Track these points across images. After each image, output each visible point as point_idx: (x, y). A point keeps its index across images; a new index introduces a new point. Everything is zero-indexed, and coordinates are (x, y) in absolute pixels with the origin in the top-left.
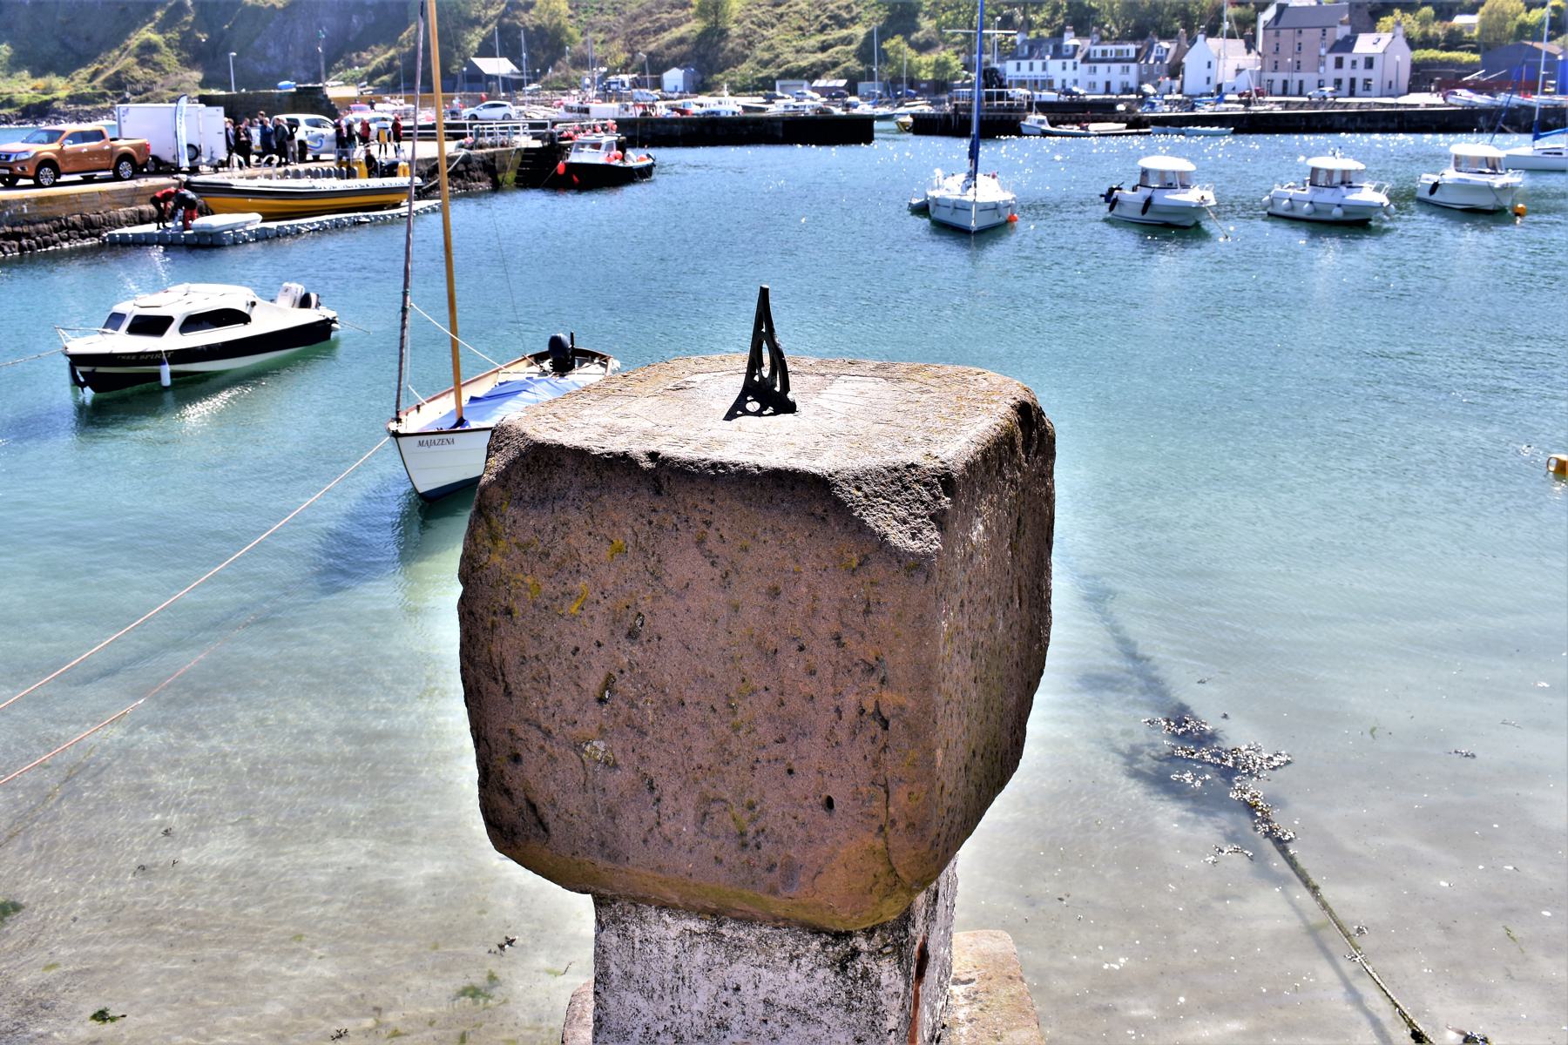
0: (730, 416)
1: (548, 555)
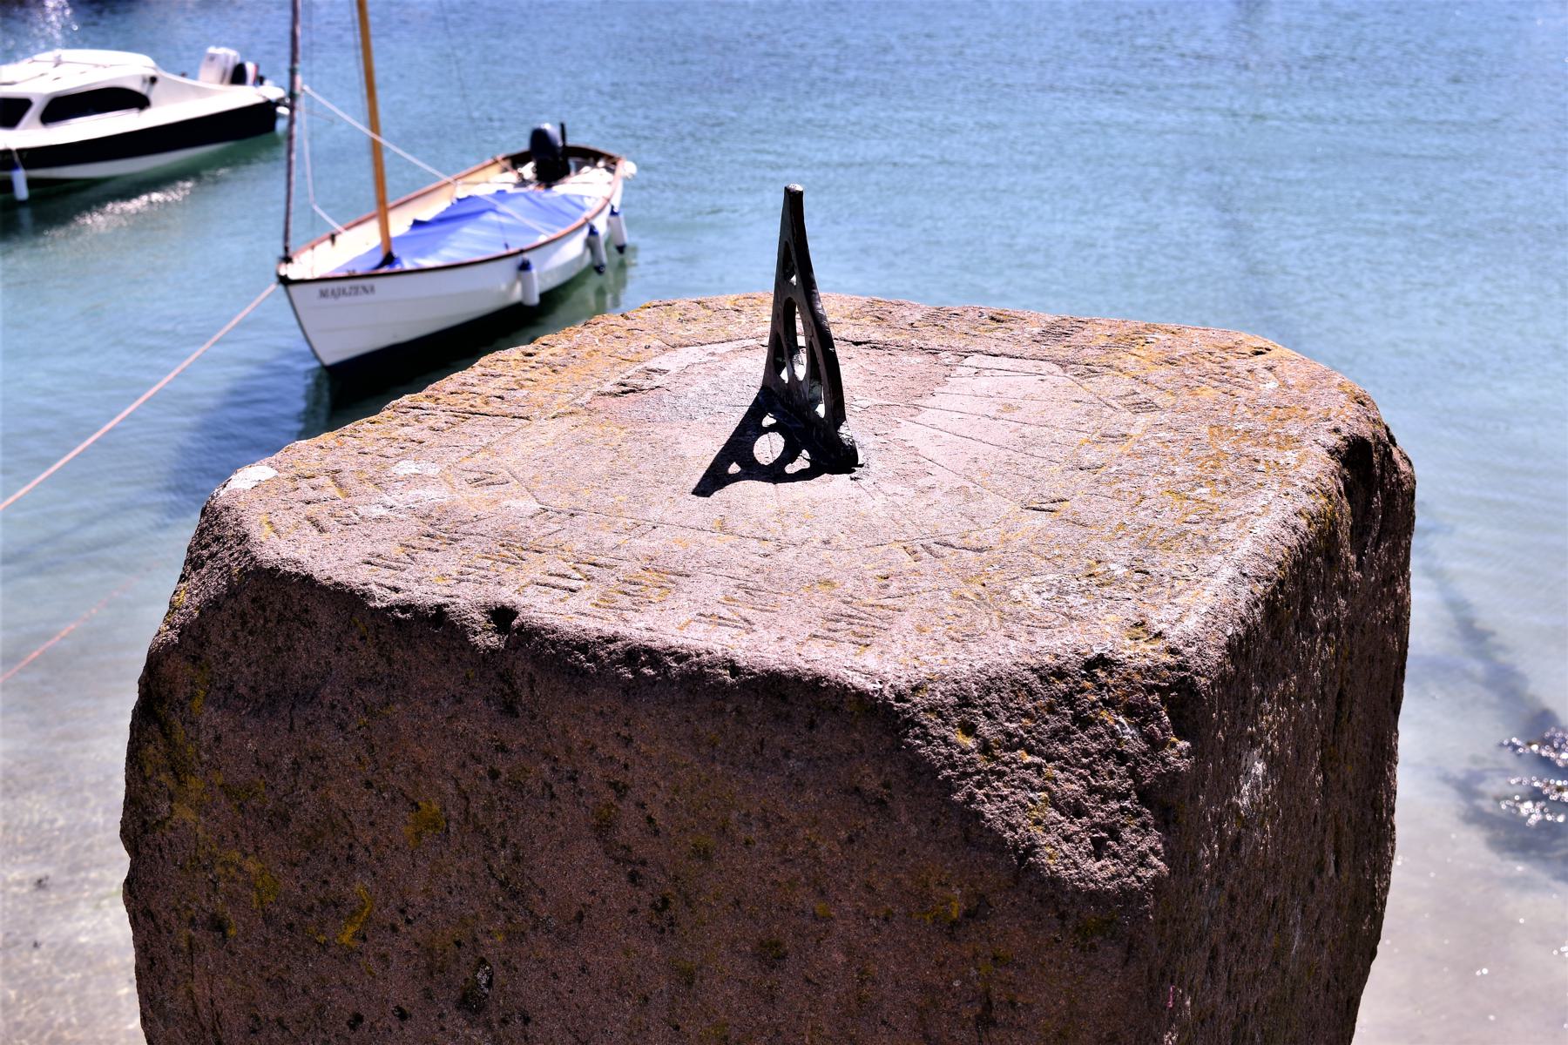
0: (713, 481)
1: (286, 819)
